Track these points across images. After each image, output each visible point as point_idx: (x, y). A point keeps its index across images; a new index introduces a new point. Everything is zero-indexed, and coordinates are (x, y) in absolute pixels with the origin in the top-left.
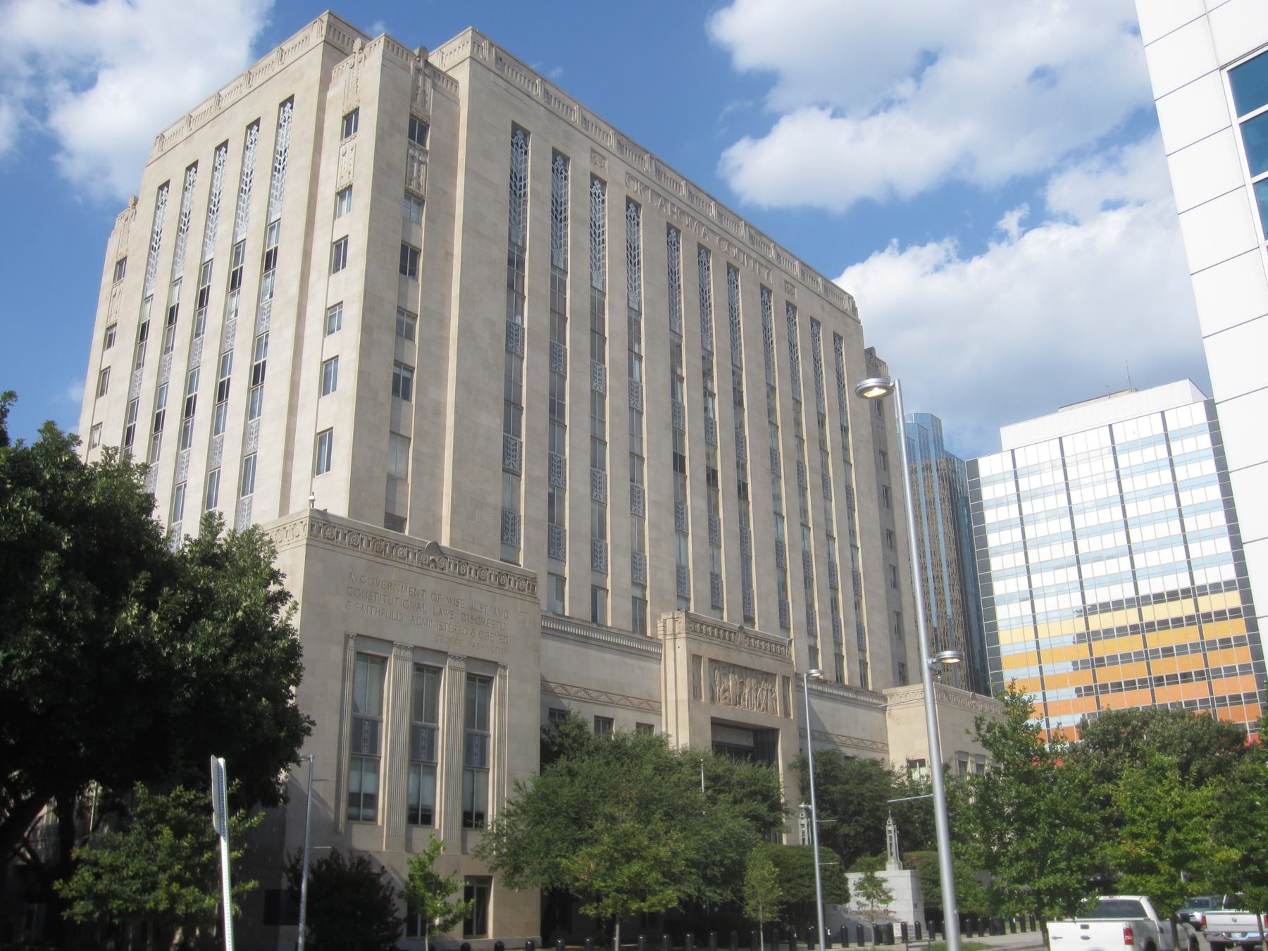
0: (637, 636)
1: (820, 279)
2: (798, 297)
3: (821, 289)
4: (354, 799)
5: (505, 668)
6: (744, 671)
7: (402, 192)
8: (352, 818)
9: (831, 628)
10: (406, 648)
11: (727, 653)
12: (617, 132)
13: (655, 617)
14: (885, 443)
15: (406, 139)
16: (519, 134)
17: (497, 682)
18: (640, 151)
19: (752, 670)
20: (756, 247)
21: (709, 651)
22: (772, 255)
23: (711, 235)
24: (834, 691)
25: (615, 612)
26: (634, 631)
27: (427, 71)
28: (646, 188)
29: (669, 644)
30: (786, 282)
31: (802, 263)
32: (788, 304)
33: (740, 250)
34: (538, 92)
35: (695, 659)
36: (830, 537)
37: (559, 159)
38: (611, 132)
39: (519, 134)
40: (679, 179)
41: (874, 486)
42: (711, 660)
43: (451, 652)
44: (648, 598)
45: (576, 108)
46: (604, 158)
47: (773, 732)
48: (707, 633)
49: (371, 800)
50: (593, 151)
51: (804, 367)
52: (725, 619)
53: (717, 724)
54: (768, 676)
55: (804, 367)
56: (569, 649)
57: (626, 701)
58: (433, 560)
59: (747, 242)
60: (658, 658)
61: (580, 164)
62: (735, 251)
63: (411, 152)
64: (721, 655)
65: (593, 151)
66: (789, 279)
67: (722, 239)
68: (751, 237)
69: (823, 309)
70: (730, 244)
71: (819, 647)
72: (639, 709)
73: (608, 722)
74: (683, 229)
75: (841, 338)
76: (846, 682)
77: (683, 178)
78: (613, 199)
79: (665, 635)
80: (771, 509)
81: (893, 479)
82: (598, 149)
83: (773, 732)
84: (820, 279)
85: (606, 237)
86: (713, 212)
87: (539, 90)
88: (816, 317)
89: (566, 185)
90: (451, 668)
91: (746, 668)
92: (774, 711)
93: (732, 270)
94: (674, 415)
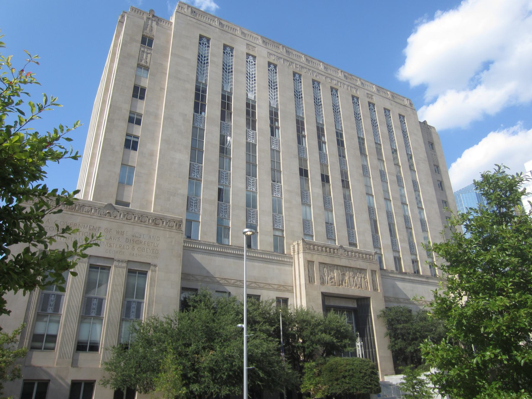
0: (275, 253)
1: (389, 93)
2: (376, 100)
3: (390, 96)
4: (37, 338)
5: (155, 266)
6: (344, 268)
7: (136, 65)
8: (33, 348)
9: (408, 247)
10: (122, 261)
11: (324, 256)
12: (305, 55)
13: (289, 245)
14: (438, 161)
15: (139, 44)
16: (204, 41)
17: (149, 274)
18: (277, 45)
19: (350, 267)
20: (348, 80)
21: (317, 258)
22: (359, 83)
23: (320, 76)
24: (412, 278)
25: (265, 242)
26: (274, 251)
27: (153, 19)
28: (279, 58)
29: (296, 256)
30: (367, 94)
31: (376, 86)
32: (369, 103)
33: (338, 81)
34: (217, 24)
35: (309, 264)
36: (404, 204)
37: (228, 50)
38: (259, 38)
39: (204, 41)
40: (301, 55)
41: (431, 180)
42: (320, 263)
43: (116, 258)
44: (285, 236)
45: (238, 29)
46: (254, 47)
47: (367, 299)
48: (318, 250)
49: (55, 337)
50: (247, 44)
51: (382, 129)
52: (314, 240)
53: (325, 296)
54: (362, 271)
55: (382, 129)
56: (231, 261)
57: (269, 286)
58: (109, 213)
59: (343, 78)
60: (291, 264)
61: (240, 49)
62: (335, 82)
63: (142, 49)
64: (328, 260)
65: (247, 44)
66: (369, 92)
67: (326, 77)
68: (345, 76)
69: (391, 104)
70: (332, 79)
71: (401, 256)
72: (277, 290)
73: (258, 297)
74: (303, 74)
75: (404, 117)
76: (421, 274)
77: (303, 54)
78: (262, 62)
79: (294, 252)
80: (364, 192)
81: (444, 177)
82: (250, 43)
83: (367, 299)
84: (389, 93)
85: (278, 86)
86: (322, 67)
87: (239, 32)
88: (387, 108)
89: (320, 92)
90: (116, 267)
91: (346, 267)
92: (367, 288)
93: (334, 91)
94: (414, 186)
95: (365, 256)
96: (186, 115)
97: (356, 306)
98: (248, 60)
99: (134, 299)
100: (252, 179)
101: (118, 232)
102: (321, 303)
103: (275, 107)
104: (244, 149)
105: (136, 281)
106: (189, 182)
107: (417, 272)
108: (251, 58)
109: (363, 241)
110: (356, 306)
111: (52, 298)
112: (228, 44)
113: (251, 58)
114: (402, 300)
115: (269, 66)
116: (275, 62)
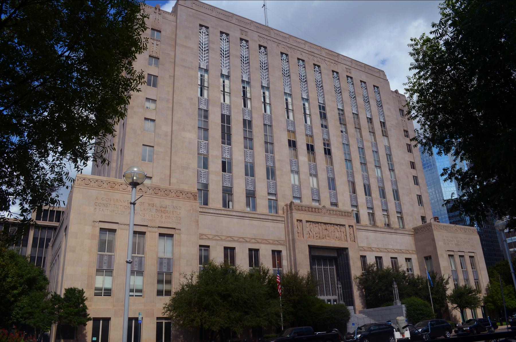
66: (347, 67)
95: (345, 214)
96: (192, 99)
97: (336, 255)
98: (222, 38)
99: (106, 253)
100: (203, 143)
101: (149, 204)
102: (308, 254)
103: (205, 68)
104: (242, 125)
105: (107, 236)
106: (198, 157)
107: (388, 225)
108: (244, 42)
109: (345, 202)
110: (336, 255)
111: (106, 258)
112: (262, 44)
113: (244, 42)
114: (374, 249)
115: (260, 49)
116: (265, 45)
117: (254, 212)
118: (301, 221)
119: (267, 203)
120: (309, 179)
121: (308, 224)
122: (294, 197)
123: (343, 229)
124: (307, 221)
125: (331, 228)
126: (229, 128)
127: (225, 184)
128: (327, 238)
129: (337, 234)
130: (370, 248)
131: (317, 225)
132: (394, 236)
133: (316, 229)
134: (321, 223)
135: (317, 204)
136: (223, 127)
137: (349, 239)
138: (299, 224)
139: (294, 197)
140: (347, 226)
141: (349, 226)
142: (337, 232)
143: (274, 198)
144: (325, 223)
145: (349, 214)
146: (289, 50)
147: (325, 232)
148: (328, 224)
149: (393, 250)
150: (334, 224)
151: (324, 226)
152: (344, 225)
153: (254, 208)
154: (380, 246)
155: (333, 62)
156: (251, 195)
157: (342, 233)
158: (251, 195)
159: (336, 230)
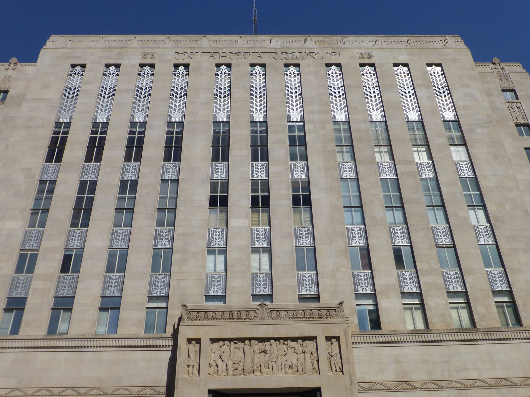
117: (115, 336)
118: (198, 341)
119: (142, 315)
120: (249, 258)
121: (217, 345)
122: (494, 292)
123: (310, 346)
124: (214, 340)
125: (274, 347)
126: (91, 201)
127: (496, 286)
128: (264, 370)
129: (293, 360)
130: (407, 383)
131: (240, 345)
132: (484, 348)
133: (234, 352)
134: (250, 339)
135: (222, 304)
136: (79, 200)
137: (324, 366)
138: (194, 347)
139: (494, 292)
140: (321, 340)
141: (329, 339)
142: (293, 355)
143: (164, 305)
144: (262, 340)
145: (333, 312)
146: (232, 56)
147: (260, 358)
148: (268, 339)
149: (482, 380)
150: (286, 339)
151: (258, 346)
152: (313, 339)
153: (114, 325)
154: (437, 376)
155: (330, 50)
156: (110, 305)
157: (308, 356)
158: (110, 305)
159: (291, 351)
